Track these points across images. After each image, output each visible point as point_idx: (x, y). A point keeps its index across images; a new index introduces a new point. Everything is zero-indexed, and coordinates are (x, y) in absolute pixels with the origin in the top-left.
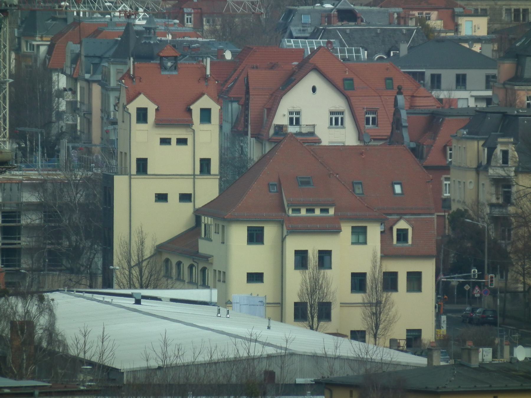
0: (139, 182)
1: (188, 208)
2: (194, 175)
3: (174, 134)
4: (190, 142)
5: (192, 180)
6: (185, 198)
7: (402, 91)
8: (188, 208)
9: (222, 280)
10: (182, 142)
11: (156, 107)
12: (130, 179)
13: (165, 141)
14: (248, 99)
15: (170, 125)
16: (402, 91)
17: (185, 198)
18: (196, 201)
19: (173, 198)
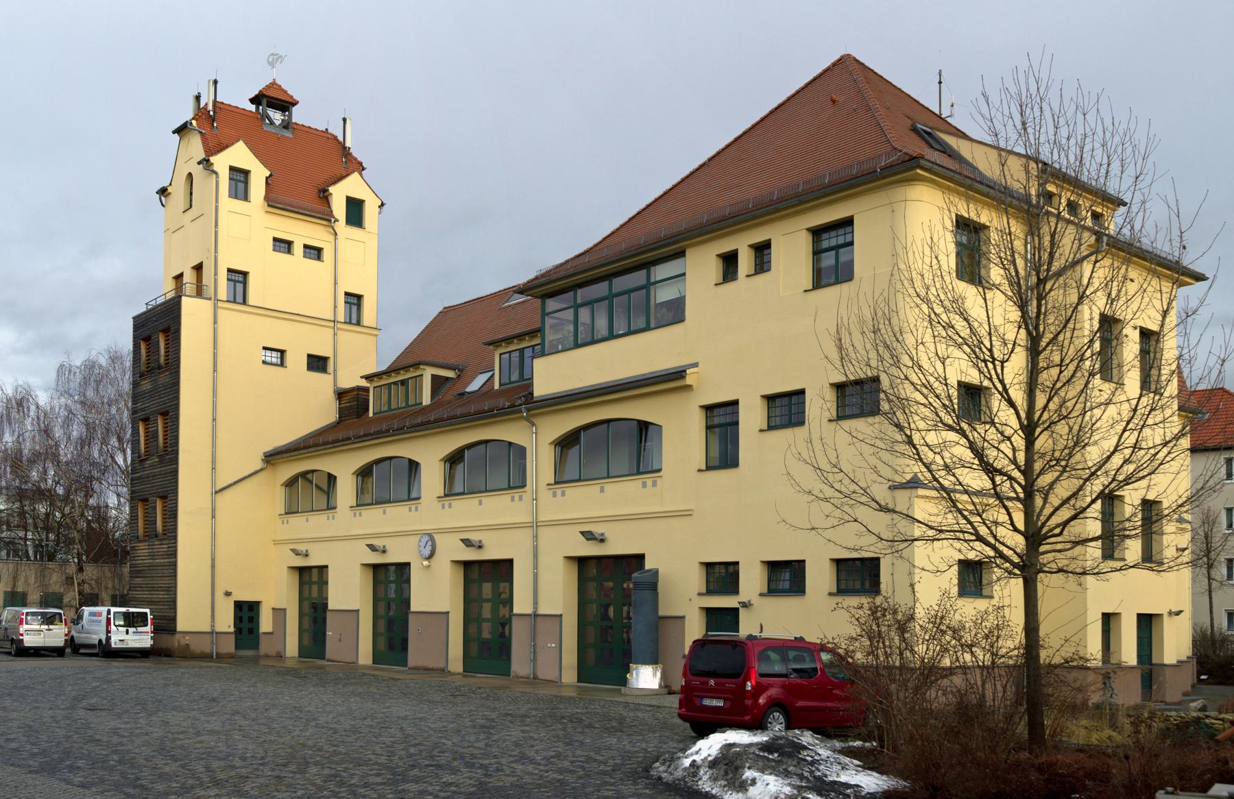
0: (231, 317)
1: (323, 385)
2: (535, 526)
3: (302, 231)
4: (327, 255)
5: (540, 519)
6: (317, 363)
7: (239, 96)
8: (323, 385)
9: (354, 321)
10: (314, 252)
11: (268, 173)
12: (215, 308)
13: (284, 245)
14: (1069, 499)
15: (422, 424)
16: (239, 96)
17: (317, 363)
18: (339, 374)
19: (297, 361)
